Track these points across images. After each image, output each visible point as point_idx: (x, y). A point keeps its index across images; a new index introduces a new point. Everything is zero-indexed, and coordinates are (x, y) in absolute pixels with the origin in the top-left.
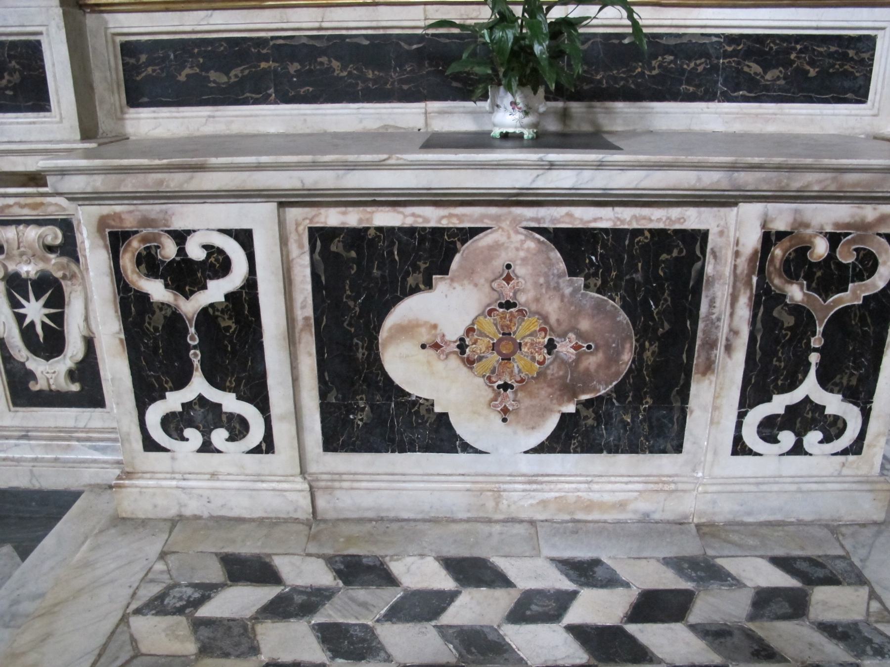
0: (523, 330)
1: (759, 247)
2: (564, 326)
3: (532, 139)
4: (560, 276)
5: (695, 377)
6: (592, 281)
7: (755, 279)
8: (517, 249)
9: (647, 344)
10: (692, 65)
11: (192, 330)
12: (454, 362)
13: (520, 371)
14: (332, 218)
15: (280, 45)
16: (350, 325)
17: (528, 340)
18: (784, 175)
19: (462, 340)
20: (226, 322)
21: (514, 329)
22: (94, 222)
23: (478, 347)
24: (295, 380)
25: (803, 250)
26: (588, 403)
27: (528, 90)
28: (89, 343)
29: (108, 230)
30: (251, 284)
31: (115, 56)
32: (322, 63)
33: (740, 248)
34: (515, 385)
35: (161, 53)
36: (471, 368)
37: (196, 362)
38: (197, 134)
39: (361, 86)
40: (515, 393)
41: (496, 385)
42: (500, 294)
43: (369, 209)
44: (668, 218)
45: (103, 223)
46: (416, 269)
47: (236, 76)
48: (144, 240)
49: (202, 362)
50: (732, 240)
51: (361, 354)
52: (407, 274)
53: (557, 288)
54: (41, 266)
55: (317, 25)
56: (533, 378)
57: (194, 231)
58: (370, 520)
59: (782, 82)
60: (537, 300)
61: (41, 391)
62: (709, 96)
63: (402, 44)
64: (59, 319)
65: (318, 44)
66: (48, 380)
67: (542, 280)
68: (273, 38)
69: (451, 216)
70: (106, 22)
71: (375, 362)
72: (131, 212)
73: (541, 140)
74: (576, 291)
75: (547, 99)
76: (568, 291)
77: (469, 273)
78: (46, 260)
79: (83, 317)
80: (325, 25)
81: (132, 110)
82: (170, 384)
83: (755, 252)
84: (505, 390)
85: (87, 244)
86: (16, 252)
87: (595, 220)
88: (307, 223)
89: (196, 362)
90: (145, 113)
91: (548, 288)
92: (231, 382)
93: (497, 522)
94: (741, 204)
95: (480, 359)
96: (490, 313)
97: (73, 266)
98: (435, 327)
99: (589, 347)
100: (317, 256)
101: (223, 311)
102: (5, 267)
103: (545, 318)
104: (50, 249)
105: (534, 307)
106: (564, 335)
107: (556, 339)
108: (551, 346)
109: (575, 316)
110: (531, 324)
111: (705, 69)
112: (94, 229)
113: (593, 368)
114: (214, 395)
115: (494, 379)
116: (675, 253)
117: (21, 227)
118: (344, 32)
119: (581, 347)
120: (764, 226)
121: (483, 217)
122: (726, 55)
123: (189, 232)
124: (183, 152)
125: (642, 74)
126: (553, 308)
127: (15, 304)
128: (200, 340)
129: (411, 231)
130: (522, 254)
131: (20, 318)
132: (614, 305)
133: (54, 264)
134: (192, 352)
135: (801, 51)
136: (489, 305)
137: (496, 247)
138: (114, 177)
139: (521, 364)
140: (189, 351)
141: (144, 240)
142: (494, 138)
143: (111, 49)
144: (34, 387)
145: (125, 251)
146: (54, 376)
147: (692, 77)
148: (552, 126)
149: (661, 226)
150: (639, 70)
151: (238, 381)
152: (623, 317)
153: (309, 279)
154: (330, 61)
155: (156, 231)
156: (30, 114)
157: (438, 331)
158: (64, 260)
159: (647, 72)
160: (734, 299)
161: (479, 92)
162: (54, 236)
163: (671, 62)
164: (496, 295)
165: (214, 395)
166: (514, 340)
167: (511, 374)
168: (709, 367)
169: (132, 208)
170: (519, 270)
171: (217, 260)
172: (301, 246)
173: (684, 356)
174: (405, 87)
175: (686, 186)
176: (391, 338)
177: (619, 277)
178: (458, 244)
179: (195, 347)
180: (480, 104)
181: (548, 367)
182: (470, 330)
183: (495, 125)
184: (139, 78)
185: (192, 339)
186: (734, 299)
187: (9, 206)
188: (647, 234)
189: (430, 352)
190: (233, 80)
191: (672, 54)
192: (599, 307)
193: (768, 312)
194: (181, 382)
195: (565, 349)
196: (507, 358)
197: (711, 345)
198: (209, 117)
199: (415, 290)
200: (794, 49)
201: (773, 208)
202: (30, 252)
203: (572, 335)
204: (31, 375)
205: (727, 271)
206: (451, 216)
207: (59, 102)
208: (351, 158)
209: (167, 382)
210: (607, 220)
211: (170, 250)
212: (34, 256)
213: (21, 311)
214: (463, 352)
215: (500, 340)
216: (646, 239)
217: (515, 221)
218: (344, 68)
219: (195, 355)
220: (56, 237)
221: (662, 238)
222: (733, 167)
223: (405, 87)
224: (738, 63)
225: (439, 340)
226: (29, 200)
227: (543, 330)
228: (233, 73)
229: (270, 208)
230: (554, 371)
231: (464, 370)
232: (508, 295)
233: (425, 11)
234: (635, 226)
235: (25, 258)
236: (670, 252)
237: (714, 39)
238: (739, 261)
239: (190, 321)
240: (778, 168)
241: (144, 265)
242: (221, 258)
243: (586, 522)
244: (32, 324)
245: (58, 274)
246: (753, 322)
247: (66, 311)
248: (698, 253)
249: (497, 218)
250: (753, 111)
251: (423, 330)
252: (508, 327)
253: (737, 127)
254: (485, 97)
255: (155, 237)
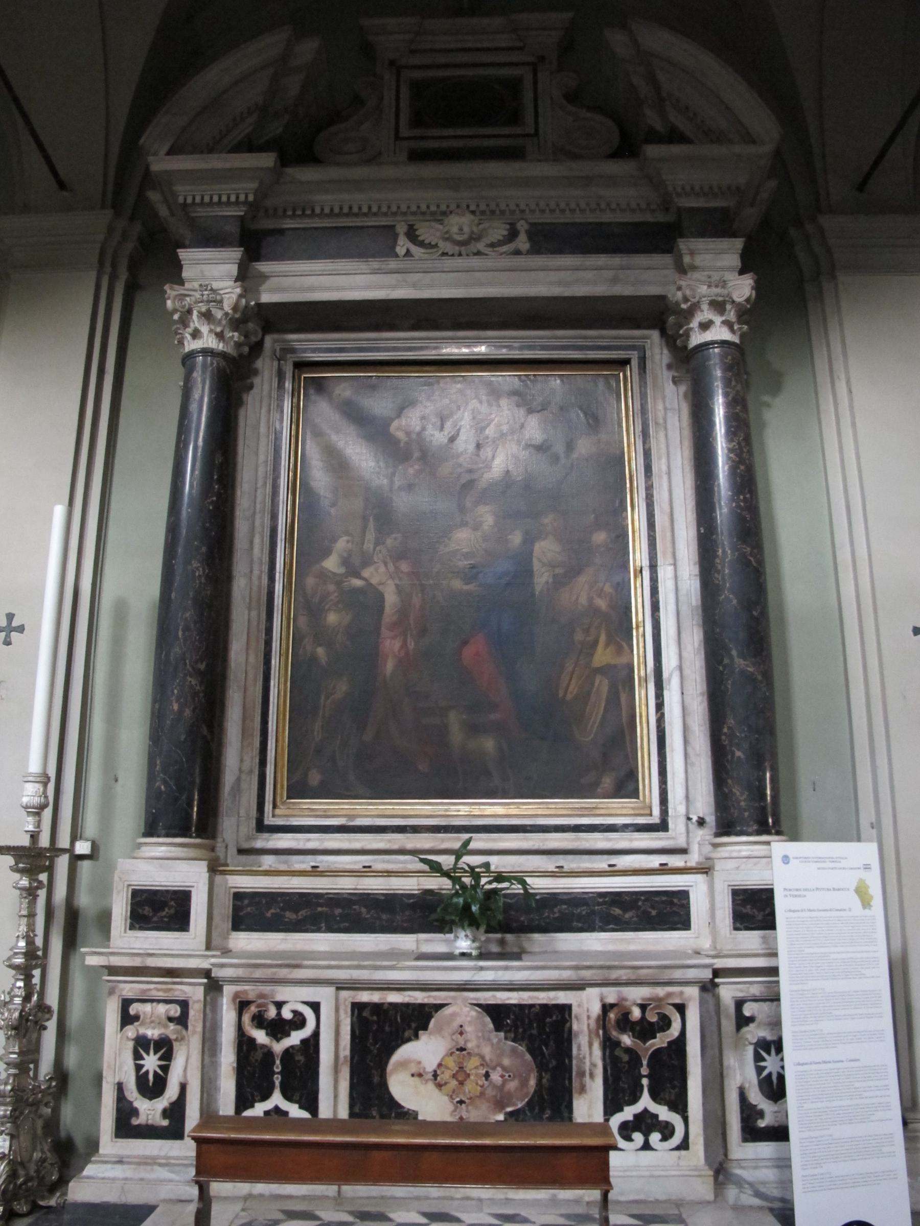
0: (471, 1064)
1: (601, 1013)
2: (494, 1064)
3: (478, 956)
4: (490, 1032)
5: (575, 1096)
6: (508, 1035)
7: (601, 1032)
8: (466, 1016)
9: (544, 1074)
10: (579, 911)
11: (278, 1062)
12: (431, 1086)
13: (470, 1092)
14: (365, 997)
15: (331, 898)
16: (371, 1061)
17: (473, 1071)
18: (606, 972)
19: (435, 1071)
20: (300, 1058)
21: (465, 1064)
22: (232, 995)
23: (445, 1076)
24: (336, 1096)
25: (626, 1015)
26: (511, 1114)
27: (474, 928)
28: (183, 1087)
29: (238, 1000)
30: (316, 1034)
31: (229, 900)
32: (355, 910)
33: (590, 1013)
34: (467, 1101)
35: (257, 899)
36: (440, 1090)
37: (277, 1083)
38: (275, 949)
39: (378, 923)
40: (467, 1106)
41: (455, 1101)
42: (457, 1043)
43: (385, 992)
44: (549, 998)
45: (236, 995)
46: (410, 1027)
47: (302, 915)
48: (259, 1006)
49: (282, 1084)
50: (586, 1009)
51: (376, 1080)
52: (404, 1031)
53: (489, 1040)
54: (162, 1031)
55: (354, 887)
56: (477, 1097)
57: (287, 1002)
58: (375, 1198)
59: (635, 919)
60: (478, 1046)
61: (139, 1126)
62: (591, 929)
63: (404, 899)
64: (165, 1069)
65: (353, 898)
66: (148, 1115)
67: (480, 1034)
68: (327, 894)
69: (429, 997)
70: (227, 880)
71: (384, 1085)
72: (253, 990)
73: (482, 956)
74: (500, 1041)
75: (487, 932)
76: (495, 1041)
77: (439, 1030)
78: (166, 1027)
79: (183, 1068)
80: (359, 887)
81: (234, 933)
82: (259, 1098)
83: (599, 1017)
84: (461, 1105)
85: (225, 1007)
86: (148, 1021)
87: (508, 999)
88: (351, 1000)
89: (277, 1083)
90: (242, 935)
91: (484, 1039)
92: (297, 1096)
93: (458, 1199)
94: (587, 989)
95: (446, 1083)
96: (452, 1054)
97: (184, 1032)
98: (419, 1063)
99: (509, 1076)
100: (355, 1019)
101: (298, 1051)
102: (138, 1031)
103: (482, 1057)
104: (170, 1019)
105: (476, 1051)
106: (494, 1068)
107: (490, 1071)
108: (487, 1076)
109: (501, 1055)
110: (474, 1062)
111: (587, 913)
112: (230, 998)
113: (513, 1089)
114: (285, 1105)
115: (454, 1097)
116: (554, 1018)
117: (155, 1004)
118: (370, 892)
119: (505, 1076)
120: (602, 1000)
121: (446, 998)
122: (599, 904)
123: (284, 1003)
124: (281, 958)
125: (548, 917)
126: (487, 1051)
127: (137, 1056)
128: (282, 1068)
129: (407, 1005)
130: (469, 1019)
131: (138, 1067)
132: (521, 1049)
133: (171, 1030)
134: (276, 1076)
135: (644, 901)
136: (450, 1050)
137: (454, 1015)
138: (249, 970)
139: (471, 1087)
140: (273, 1076)
141: (259, 1006)
142: (455, 955)
143: (227, 895)
144: (135, 1122)
145: (246, 1012)
146: (153, 1112)
147: (579, 918)
148: (495, 948)
149: (545, 1002)
150: (547, 914)
151: (301, 1097)
152: (528, 1057)
153: (349, 1032)
154: (360, 908)
155: (266, 1001)
156: (175, 933)
157: (422, 1066)
158: (179, 1027)
159: (552, 916)
160: (591, 1045)
161: (447, 929)
162: (175, 1010)
163: (565, 909)
164: (454, 1044)
165: (285, 1105)
166: (465, 1071)
167: (464, 1093)
168: (583, 1089)
169: (254, 987)
170: (468, 1028)
171: (298, 1019)
172: (346, 1013)
173: (567, 1082)
174: (405, 925)
175: (553, 978)
176: (395, 1069)
177: (524, 1032)
178: (433, 1013)
179: (278, 1073)
180: (448, 936)
181: (485, 1089)
182: (440, 1065)
183: (457, 948)
184: (241, 914)
185: (277, 1068)
186: (591, 1045)
187: (150, 990)
188: (538, 1007)
189: (417, 1079)
190: (300, 917)
191: (565, 904)
192: (514, 1051)
193: (612, 1053)
194: (265, 1097)
195: (496, 1077)
196: (461, 1083)
197: (582, 1074)
198: (283, 939)
199: (409, 1040)
200: (640, 899)
201: (605, 990)
202: (157, 1021)
203: (499, 1069)
204: (135, 1112)
205: (585, 1028)
206: (429, 997)
207: (196, 926)
208: (378, 963)
209: (257, 1096)
210: (515, 999)
211: (272, 1013)
212: (159, 1023)
213: (142, 1062)
214: (436, 1079)
215: (457, 1072)
216: (538, 1009)
217: (465, 999)
218: (368, 912)
219: (277, 1078)
220: (176, 1012)
221: (547, 1009)
222: (577, 968)
223: (405, 925)
224: (607, 909)
225: (421, 1071)
226: (164, 987)
227: (482, 1065)
228: (300, 914)
229: (331, 990)
230: (490, 1092)
231: (436, 1091)
232: (461, 1043)
233: (418, 881)
234: (531, 1002)
235: (153, 1025)
236: (551, 1017)
237: (591, 895)
238: (590, 1021)
239: (278, 1057)
240: (601, 967)
241: (256, 1021)
242: (301, 1018)
243: (514, 1200)
244: (147, 1072)
245: (173, 1037)
246: (604, 1059)
247: (173, 1063)
248: (567, 1016)
249: (454, 998)
250: (619, 937)
251: (413, 1065)
252: (462, 1063)
253: (611, 947)
254: (450, 931)
255: (265, 1005)
